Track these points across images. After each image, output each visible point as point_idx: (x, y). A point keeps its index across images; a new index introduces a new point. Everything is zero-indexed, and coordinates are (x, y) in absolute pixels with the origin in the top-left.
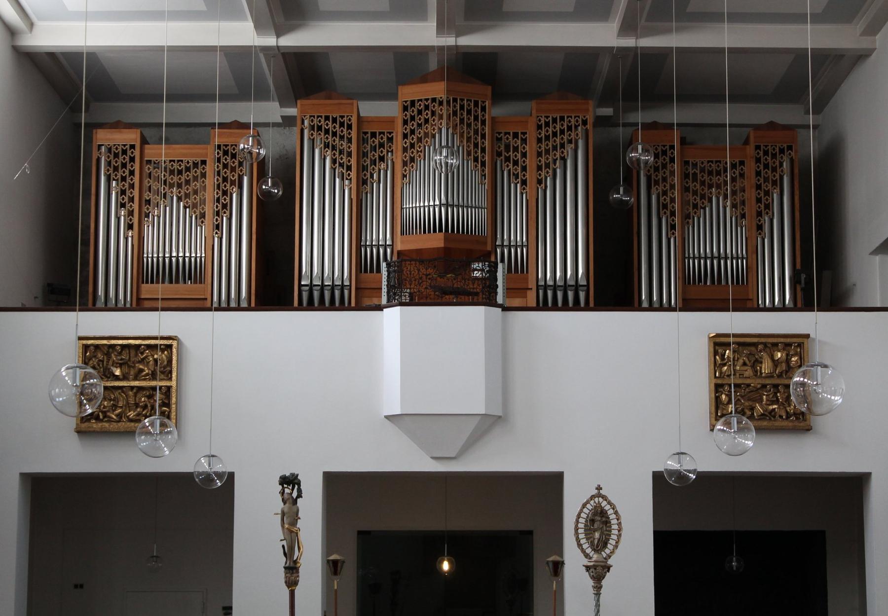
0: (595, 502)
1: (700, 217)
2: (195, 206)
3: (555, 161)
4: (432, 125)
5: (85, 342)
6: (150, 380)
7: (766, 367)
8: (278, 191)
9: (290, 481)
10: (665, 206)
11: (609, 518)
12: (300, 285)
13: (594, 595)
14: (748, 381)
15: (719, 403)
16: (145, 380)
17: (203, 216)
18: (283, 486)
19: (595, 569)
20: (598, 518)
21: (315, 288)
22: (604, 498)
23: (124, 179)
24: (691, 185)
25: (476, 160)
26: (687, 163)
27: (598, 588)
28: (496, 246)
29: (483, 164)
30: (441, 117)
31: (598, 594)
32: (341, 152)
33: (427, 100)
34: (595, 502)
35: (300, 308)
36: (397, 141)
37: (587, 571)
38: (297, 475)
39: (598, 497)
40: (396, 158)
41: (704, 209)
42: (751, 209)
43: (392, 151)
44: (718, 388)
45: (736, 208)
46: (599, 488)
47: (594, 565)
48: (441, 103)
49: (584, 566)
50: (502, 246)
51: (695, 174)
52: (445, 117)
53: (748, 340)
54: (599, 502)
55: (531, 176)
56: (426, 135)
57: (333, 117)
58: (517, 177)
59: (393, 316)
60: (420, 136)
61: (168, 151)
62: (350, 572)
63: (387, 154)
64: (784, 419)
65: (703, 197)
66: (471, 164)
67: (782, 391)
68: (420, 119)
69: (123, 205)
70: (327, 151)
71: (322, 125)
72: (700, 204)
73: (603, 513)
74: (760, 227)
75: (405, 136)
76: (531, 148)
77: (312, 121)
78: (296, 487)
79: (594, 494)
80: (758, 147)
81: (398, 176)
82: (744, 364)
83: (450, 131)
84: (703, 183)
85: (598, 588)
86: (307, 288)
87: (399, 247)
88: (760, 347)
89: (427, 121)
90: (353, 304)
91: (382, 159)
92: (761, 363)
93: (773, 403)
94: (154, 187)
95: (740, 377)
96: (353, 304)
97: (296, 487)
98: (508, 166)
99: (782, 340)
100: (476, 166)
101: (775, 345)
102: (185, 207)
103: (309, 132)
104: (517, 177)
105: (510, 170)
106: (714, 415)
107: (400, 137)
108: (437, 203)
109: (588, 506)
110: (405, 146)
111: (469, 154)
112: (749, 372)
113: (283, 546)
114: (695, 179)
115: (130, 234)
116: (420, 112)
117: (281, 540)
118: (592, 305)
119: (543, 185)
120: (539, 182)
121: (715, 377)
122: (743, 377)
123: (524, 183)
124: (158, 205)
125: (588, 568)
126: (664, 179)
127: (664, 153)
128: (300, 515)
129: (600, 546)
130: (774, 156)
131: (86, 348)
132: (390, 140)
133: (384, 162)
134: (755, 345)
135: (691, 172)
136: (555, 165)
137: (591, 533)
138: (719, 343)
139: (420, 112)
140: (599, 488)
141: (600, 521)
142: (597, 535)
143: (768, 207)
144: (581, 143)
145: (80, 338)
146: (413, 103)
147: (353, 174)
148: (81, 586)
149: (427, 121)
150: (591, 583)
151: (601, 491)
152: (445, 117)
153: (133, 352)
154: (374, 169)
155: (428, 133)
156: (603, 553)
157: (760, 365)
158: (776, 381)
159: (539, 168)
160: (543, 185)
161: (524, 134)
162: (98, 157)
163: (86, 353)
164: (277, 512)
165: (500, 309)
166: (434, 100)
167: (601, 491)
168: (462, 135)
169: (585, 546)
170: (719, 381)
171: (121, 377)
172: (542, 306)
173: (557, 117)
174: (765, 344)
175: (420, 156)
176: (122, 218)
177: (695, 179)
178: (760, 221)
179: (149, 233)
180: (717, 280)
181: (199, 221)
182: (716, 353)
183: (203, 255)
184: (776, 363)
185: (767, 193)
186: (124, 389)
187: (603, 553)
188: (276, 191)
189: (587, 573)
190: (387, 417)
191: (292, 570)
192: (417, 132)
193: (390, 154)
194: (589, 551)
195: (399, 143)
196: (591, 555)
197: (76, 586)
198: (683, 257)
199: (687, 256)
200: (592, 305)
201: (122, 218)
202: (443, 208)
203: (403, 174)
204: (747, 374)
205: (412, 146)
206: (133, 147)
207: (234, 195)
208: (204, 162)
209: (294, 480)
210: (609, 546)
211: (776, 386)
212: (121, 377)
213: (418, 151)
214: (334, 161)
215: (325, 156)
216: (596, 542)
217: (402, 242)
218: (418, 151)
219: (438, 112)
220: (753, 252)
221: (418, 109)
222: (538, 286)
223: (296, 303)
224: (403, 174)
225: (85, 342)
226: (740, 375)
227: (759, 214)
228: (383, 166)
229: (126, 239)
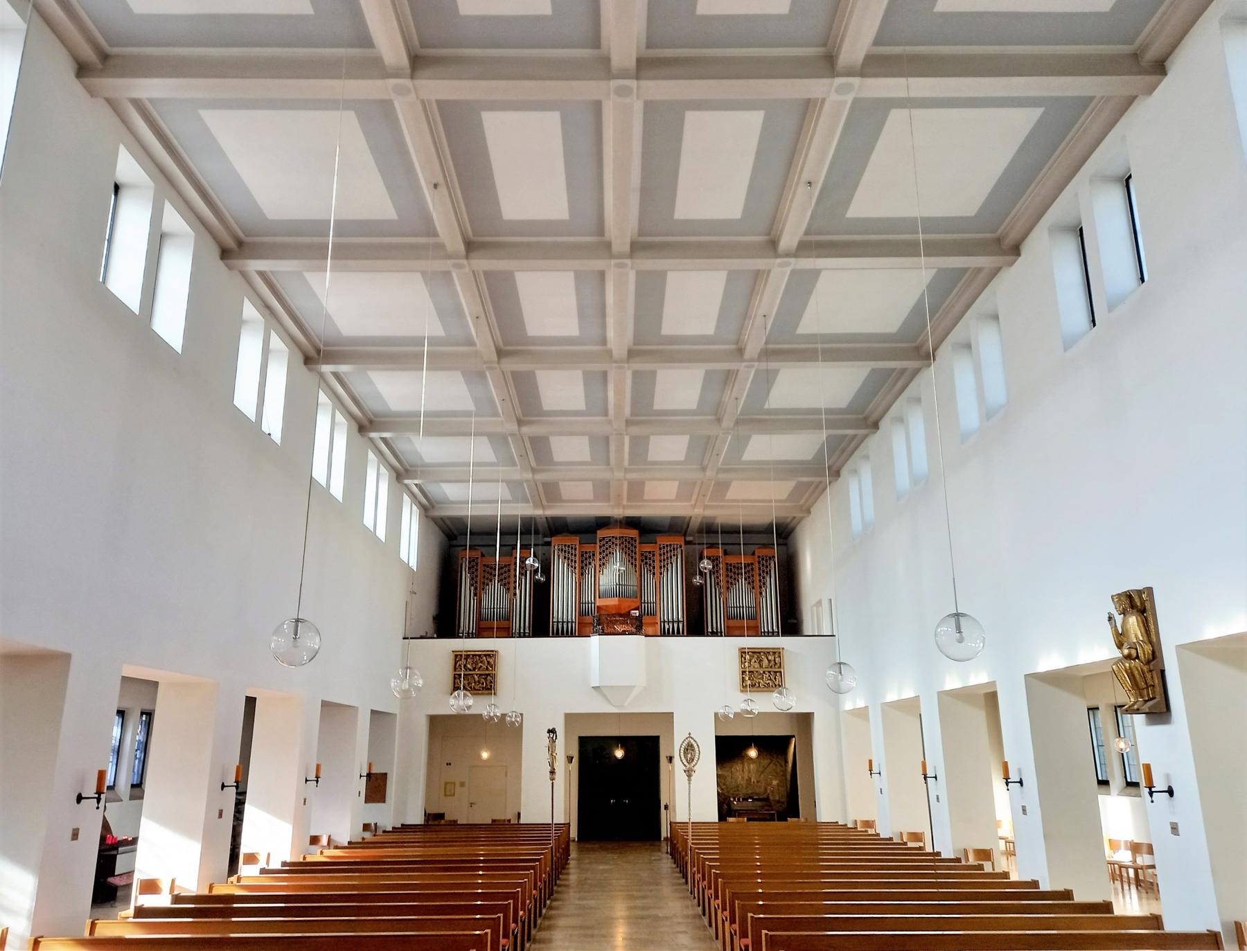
2: (505, 584)
10: (718, 584)
12: (553, 622)
14: (757, 670)
17: (508, 589)
20: (689, 748)
22: (692, 738)
24: (729, 573)
25: (632, 564)
26: (727, 564)
27: (689, 780)
29: (636, 566)
31: (689, 783)
32: (572, 561)
35: (553, 636)
42: (757, 584)
44: (743, 672)
46: (690, 734)
48: (616, 539)
51: (731, 569)
53: (756, 650)
55: (657, 571)
56: (610, 553)
58: (650, 571)
59: (595, 639)
61: (417, 349)
66: (630, 566)
69: (472, 585)
72: (734, 583)
74: (761, 593)
75: (600, 553)
76: (657, 558)
80: (759, 557)
81: (597, 571)
82: (755, 662)
84: (735, 573)
85: (689, 780)
87: (598, 604)
88: (762, 654)
90: (577, 634)
91: (590, 564)
93: (768, 680)
94: (486, 576)
96: (577, 634)
101: (769, 653)
104: (650, 571)
111: (629, 561)
112: (757, 665)
114: (731, 571)
116: (607, 543)
118: (685, 634)
120: (661, 574)
123: (654, 574)
124: (488, 584)
126: (717, 571)
129: (691, 761)
131: (456, 656)
132: (594, 555)
134: (759, 653)
138: (743, 652)
139: (607, 543)
140: (690, 734)
143: (764, 584)
144: (679, 556)
146: (604, 538)
147: (577, 571)
148: (450, 764)
149: (610, 547)
150: (687, 778)
153: (477, 657)
158: (770, 670)
161: (654, 552)
166: (613, 537)
168: (626, 553)
172: (665, 633)
185: (764, 578)
190: (593, 687)
195: (598, 556)
198: (726, 607)
200: (685, 634)
205: (604, 558)
206: (477, 558)
214: (568, 565)
217: (599, 602)
223: (551, 635)
228: (590, 566)
229: (474, 600)
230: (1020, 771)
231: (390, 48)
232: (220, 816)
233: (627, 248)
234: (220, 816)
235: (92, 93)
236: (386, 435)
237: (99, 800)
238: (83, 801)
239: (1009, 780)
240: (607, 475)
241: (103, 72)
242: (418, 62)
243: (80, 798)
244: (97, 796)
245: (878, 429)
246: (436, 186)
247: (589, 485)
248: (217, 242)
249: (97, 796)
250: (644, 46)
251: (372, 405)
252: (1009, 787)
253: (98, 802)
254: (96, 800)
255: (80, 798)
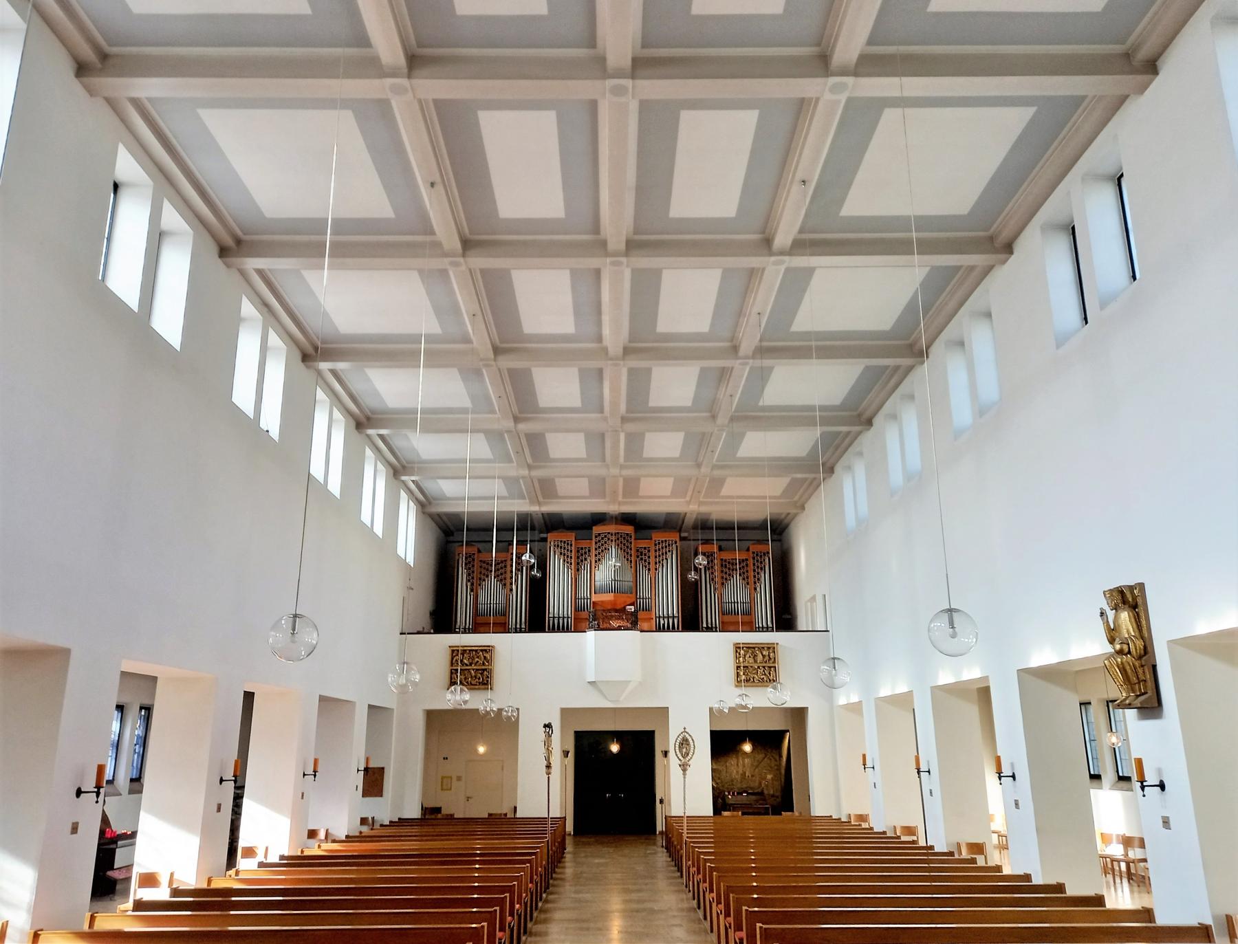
2: (501, 580)
10: (713, 579)
12: (549, 617)
14: (751, 665)
17: (505, 585)
20: (684, 742)
22: (687, 733)
23: (470, 569)
24: (724, 569)
25: (628, 560)
26: (722, 560)
27: (684, 774)
29: (631, 562)
31: (685, 778)
32: (568, 556)
35: (549, 631)
42: (751, 580)
44: (738, 667)
46: (685, 728)
48: (612, 535)
51: (726, 565)
53: (751, 646)
55: (652, 566)
56: (605, 549)
58: (646, 567)
59: (591, 635)
66: (626, 562)
69: (469, 581)
72: (728, 578)
74: (755, 589)
75: (596, 549)
76: (652, 554)
81: (593, 567)
82: (750, 657)
84: (729, 569)
85: (684, 774)
87: (593, 599)
88: (756, 649)
90: (573, 630)
91: (586, 559)
93: (763, 675)
94: (483, 572)
96: (573, 630)
101: (763, 648)
104: (646, 567)
111: (625, 557)
112: (751, 660)
114: (726, 567)
116: (602, 539)
118: (680, 629)
120: (656, 569)
123: (649, 570)
124: (484, 580)
127: (712, 555)
129: (686, 755)
130: (761, 557)
131: (453, 651)
132: (589, 551)
134: (754, 648)
138: (737, 648)
139: (602, 539)
140: (685, 728)
144: (674, 552)
146: (599, 534)
147: (573, 567)
148: (447, 758)
149: (606, 543)
150: (682, 772)
158: (764, 665)
159: (656, 563)
161: (649, 548)
166: (609, 533)
168: (621, 549)
172: (660, 629)
184: (764, 656)
185: (758, 573)
190: (589, 682)
195: (593, 552)
198: (721, 602)
200: (680, 629)
205: (599, 554)
206: (474, 554)
208: (506, 561)
214: (564, 561)
217: (595, 597)
223: (547, 630)
228: (586, 562)
229: (470, 596)
230: (1012, 765)
231: (387, 47)
232: (219, 810)
233: (623, 246)
234: (219, 810)
235: (91, 92)
236: (383, 432)
237: (98, 794)
238: (82, 795)
239: (1002, 775)
240: (602, 472)
241: (102, 72)
242: (415, 62)
243: (79, 792)
244: (96, 790)
245: (872, 425)
246: (432, 185)
247: (585, 482)
248: (215, 240)
249: (96, 790)
250: (640, 46)
251: (369, 402)
252: (1002, 782)
253: (98, 796)
254: (95, 794)
255: (79, 792)
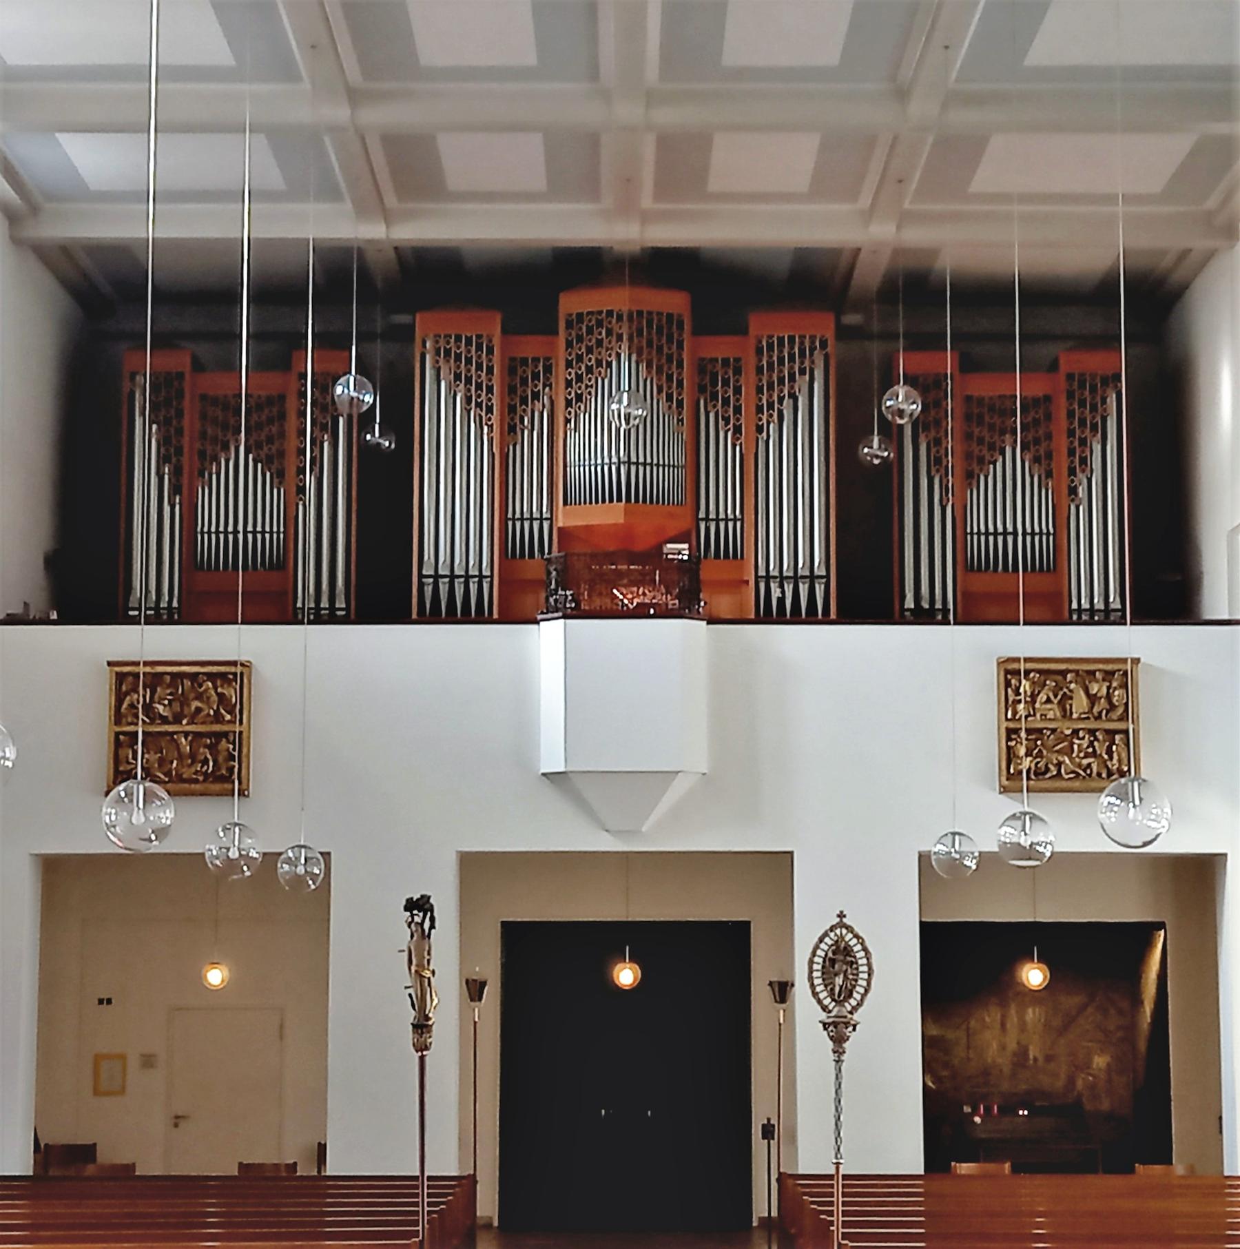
0: (836, 935)
1: (988, 474)
3: (781, 400)
4: (607, 350)
5: (118, 669)
6: (212, 723)
7: (1080, 703)
8: (390, 444)
9: (419, 906)
11: (855, 957)
12: (421, 576)
13: (834, 1063)
15: (1012, 756)
16: (203, 723)
18: (411, 913)
19: (835, 1027)
21: (441, 580)
25: (669, 398)
26: (968, 399)
27: (839, 1052)
28: (698, 520)
29: (680, 404)
30: (620, 338)
33: (600, 313)
34: (836, 935)
36: (557, 371)
37: (825, 1029)
38: (429, 898)
39: (841, 927)
40: (557, 394)
41: (994, 463)
43: (550, 386)
44: (1011, 733)
45: (1040, 464)
46: (841, 915)
47: (833, 1022)
48: (620, 318)
49: (820, 1022)
50: (707, 519)
52: (625, 337)
54: (841, 934)
56: (599, 363)
57: (466, 336)
58: (727, 421)
60: (589, 364)
62: (492, 993)
63: (544, 389)
64: (1103, 779)
65: (992, 447)
67: (1100, 737)
68: (590, 360)
70: (458, 385)
71: (451, 348)
72: (988, 457)
73: (848, 951)
74: (1073, 491)
75: (569, 364)
77: (437, 342)
78: (429, 914)
79: (834, 923)
83: (634, 357)
84: (991, 427)
85: (839, 1052)
86: (431, 580)
87: (561, 522)
89: (599, 343)
90: (496, 616)
92: (1071, 698)
95: (1041, 719)
96: (496, 616)
97: (429, 914)
98: (715, 406)
99: (1101, 666)
100: (670, 407)
102: (254, 460)
103: (433, 358)
104: (727, 421)
105: (717, 412)
106: (1004, 772)
107: (562, 364)
108: (614, 460)
109: (827, 940)
110: (569, 398)
113: (410, 995)
114: (980, 422)
115: (177, 500)
116: (590, 331)
117: (406, 988)
118: (833, 616)
119: (764, 434)
121: (1007, 719)
122: (1046, 719)
123: (737, 430)
125: (825, 1026)
128: (478, 1179)
131: (120, 677)
132: (548, 369)
133: (539, 401)
134: (1063, 673)
135: (976, 411)
136: (782, 406)
137: (831, 978)
138: (1010, 671)
139: (590, 331)
140: (841, 915)
141: (842, 961)
142: (839, 980)
143: (1083, 461)
144: (819, 374)
145: (109, 664)
146: (580, 316)
151: (845, 920)
152: (625, 337)
154: (524, 411)
155: (601, 360)
156: (846, 1004)
157: (1070, 702)
160: (764, 434)
162: (131, 389)
163: (121, 685)
164: (402, 949)
165: (705, 622)
166: (610, 313)
167: (845, 920)
168: (649, 366)
169: (822, 996)
170: (1012, 725)
171: (171, 719)
173: (784, 337)
174: (1077, 672)
175: (590, 393)
176: (166, 477)
177: (980, 422)
178: (1073, 481)
179: (204, 500)
180: (1012, 565)
181: (276, 481)
182: (1008, 684)
183: (282, 530)
184: (1093, 699)
185: (1083, 442)
186: (175, 737)
187: (846, 1004)
188: (387, 444)
189: (825, 1032)
190: (544, 774)
191: (422, 1027)
192: (585, 359)
193: (547, 389)
194: (827, 1001)
196: (831, 1007)
197: (101, 1002)
199: (969, 531)
201: (166, 477)
202: (622, 467)
203: (566, 418)
204: (1051, 715)
207: (326, 445)
209: (424, 904)
210: (855, 995)
211: (1092, 732)
212: (171, 719)
213: (587, 386)
215: (455, 391)
216: (837, 989)
217: (565, 515)
218: (587, 386)
219: (616, 329)
220: (1061, 520)
221: (587, 365)
222: (757, 577)
223: (414, 616)
224: (566, 418)
225: (118, 669)
226: (1041, 715)
227: (1072, 472)
